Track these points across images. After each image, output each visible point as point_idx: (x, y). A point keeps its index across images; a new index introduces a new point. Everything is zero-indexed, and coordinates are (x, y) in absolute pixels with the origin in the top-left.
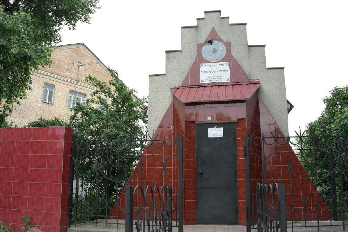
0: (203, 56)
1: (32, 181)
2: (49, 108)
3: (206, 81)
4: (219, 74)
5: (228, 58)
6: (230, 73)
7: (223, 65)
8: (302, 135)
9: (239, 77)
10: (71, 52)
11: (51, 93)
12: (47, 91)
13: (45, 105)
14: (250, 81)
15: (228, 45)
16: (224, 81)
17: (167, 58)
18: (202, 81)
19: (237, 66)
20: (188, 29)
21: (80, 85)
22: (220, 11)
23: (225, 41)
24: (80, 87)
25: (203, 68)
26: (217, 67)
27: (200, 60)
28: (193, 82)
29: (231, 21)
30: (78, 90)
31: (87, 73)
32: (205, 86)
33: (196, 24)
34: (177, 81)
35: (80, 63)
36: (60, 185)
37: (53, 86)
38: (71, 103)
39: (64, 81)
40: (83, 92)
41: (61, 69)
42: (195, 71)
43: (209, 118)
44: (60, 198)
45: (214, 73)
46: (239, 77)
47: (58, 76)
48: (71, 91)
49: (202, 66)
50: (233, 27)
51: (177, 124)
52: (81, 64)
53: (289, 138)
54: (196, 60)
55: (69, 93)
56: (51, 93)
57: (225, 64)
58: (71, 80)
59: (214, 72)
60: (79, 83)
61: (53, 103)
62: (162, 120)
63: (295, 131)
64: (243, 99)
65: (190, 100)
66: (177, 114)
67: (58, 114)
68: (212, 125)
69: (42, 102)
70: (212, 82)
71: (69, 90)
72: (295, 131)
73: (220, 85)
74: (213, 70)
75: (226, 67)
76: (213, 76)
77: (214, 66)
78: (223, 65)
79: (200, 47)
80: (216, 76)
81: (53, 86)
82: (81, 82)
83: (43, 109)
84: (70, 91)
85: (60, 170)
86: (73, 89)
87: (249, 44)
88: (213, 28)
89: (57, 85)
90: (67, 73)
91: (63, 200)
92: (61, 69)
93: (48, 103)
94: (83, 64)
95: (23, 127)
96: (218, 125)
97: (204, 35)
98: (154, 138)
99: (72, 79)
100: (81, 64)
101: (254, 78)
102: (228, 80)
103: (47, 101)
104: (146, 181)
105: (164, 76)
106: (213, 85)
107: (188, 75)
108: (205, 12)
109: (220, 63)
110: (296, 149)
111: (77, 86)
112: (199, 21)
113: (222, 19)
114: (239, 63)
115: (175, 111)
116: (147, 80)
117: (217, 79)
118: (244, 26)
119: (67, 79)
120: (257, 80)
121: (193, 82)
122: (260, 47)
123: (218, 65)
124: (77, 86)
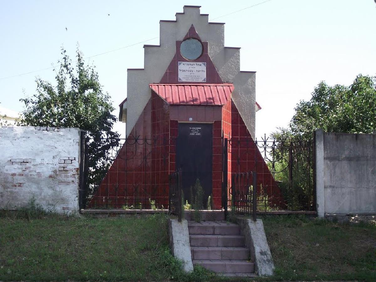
4: (196, 74)
7: (201, 65)
8: (266, 140)
20: (169, 23)
25: (182, 66)
27: (178, 58)
29: (210, 21)
38: (104, 211)
49: (180, 64)
50: (212, 25)
53: (256, 142)
54: (175, 57)
57: (202, 65)
59: (191, 85)
74: (191, 69)
76: (190, 75)
78: (201, 65)
79: (178, 44)
88: (192, 25)
95: (347, 82)
97: (183, 31)
104: (109, 184)
106: (191, 84)
107: (166, 73)
110: (267, 156)
112: (187, 8)
113: (201, 16)
116: (126, 74)
117: (193, 79)
123: (195, 64)
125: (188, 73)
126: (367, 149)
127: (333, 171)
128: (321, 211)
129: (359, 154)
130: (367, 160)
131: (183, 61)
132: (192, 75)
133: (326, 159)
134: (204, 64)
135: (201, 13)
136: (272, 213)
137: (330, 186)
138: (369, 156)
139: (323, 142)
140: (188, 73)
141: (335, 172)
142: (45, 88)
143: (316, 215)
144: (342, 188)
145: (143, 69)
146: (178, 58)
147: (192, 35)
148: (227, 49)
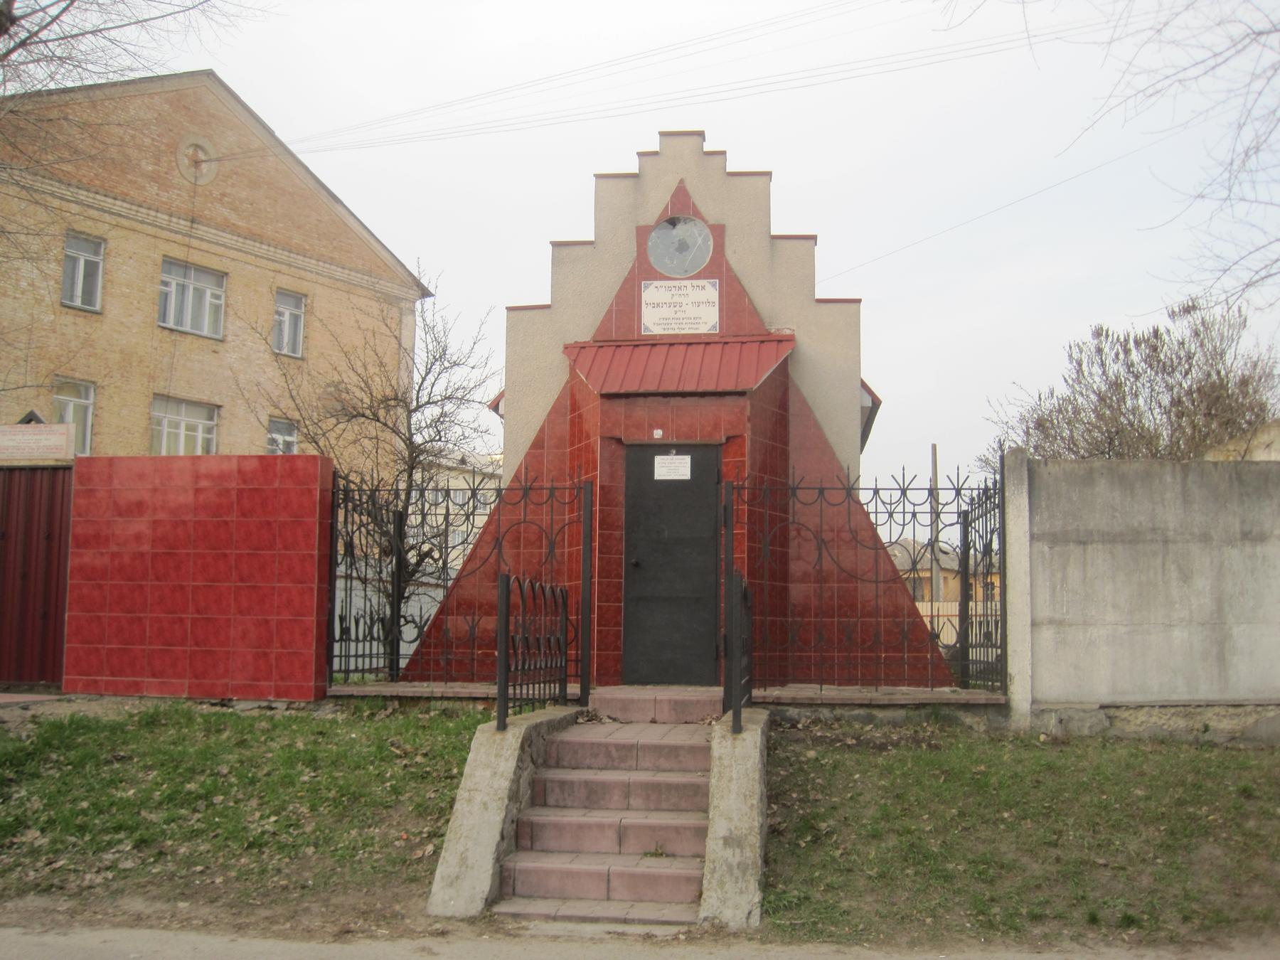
0: (652, 260)
1: (242, 580)
2: (88, 330)
3: (657, 331)
5: (718, 269)
6: (721, 310)
9: (743, 326)
10: (166, 107)
11: (91, 269)
12: (74, 260)
13: (68, 319)
14: (769, 334)
15: (719, 232)
16: (703, 329)
17: (556, 262)
18: (647, 328)
19: (373, 838)
21: (202, 240)
22: (701, 134)
23: (712, 222)
24: (205, 246)
25: (652, 293)
26: (684, 292)
27: (643, 271)
28: (619, 335)
30: (196, 257)
31: (228, 191)
32: (654, 343)
33: (634, 169)
34: (583, 329)
35: (202, 149)
36: (311, 589)
37: (96, 243)
39: (142, 222)
40: (214, 263)
41: (129, 177)
42: (627, 302)
43: (658, 434)
44: (314, 618)
45: (677, 308)
46: (743, 326)
47: (118, 203)
48: (170, 263)
49: (646, 287)
51: (580, 442)
52: (206, 153)
54: (632, 271)
55: (163, 272)
56: (91, 269)
57: (708, 287)
58: (166, 217)
59: (681, 308)
60: (201, 230)
61: (103, 307)
62: (542, 430)
63: (934, 447)
64: (739, 389)
65: (615, 390)
66: (580, 416)
67: (122, 351)
68: (664, 449)
69: (57, 306)
70: (671, 332)
71: (160, 259)
72: (934, 447)
73: (690, 342)
74: (676, 299)
75: (709, 292)
77: (680, 288)
78: (703, 288)
79: (642, 234)
80: (683, 315)
81: (96, 243)
82: (209, 226)
83: (63, 334)
84: (164, 261)
85: (312, 556)
86: (178, 253)
87: (773, 233)
88: (682, 181)
89: (117, 241)
90: (152, 189)
91: (318, 623)
92: (129, 177)
93: (80, 310)
94: (213, 154)
96: (681, 449)
97: (657, 202)
98: (450, 391)
99: (171, 215)
100: (206, 153)
101: (780, 324)
102: (714, 327)
103: (78, 302)
105: (546, 311)
107: (609, 312)
108: (663, 134)
109: (695, 282)
111: (195, 243)
114: (745, 282)
115: (575, 407)
116: (498, 325)
118: (764, 179)
119: (152, 213)
120: (788, 332)
121: (619, 335)
122: (803, 242)
124: (195, 243)
125: (666, 312)
126: (1164, 506)
127: (1059, 575)
128: (1020, 695)
129: (1140, 523)
130: (1166, 542)
131: (656, 279)
132: (679, 315)
133: (1038, 540)
134: (714, 285)
135: (730, 168)
136: (405, 343)
137: (1051, 622)
138: (1171, 526)
139: (1026, 486)
140: (666, 312)
141: (1064, 579)
142: (1238, 46)
143: (1004, 708)
144: (1086, 623)
145: (548, 307)
146: (643, 271)
147: (679, 212)
148: (778, 241)
